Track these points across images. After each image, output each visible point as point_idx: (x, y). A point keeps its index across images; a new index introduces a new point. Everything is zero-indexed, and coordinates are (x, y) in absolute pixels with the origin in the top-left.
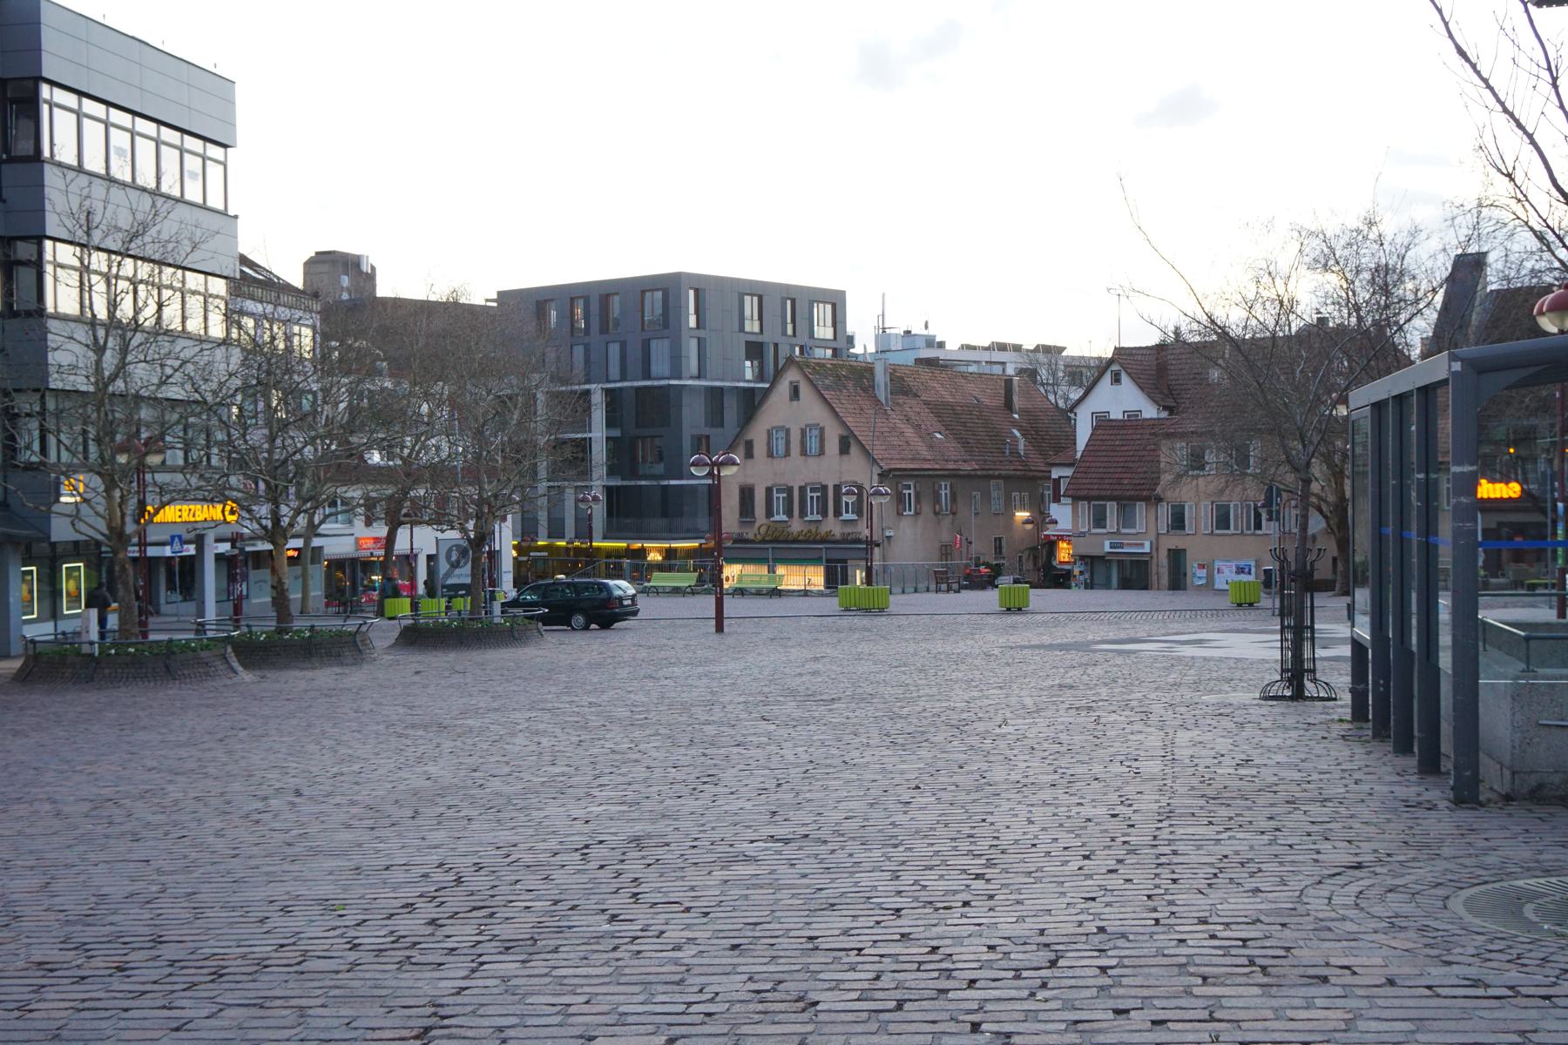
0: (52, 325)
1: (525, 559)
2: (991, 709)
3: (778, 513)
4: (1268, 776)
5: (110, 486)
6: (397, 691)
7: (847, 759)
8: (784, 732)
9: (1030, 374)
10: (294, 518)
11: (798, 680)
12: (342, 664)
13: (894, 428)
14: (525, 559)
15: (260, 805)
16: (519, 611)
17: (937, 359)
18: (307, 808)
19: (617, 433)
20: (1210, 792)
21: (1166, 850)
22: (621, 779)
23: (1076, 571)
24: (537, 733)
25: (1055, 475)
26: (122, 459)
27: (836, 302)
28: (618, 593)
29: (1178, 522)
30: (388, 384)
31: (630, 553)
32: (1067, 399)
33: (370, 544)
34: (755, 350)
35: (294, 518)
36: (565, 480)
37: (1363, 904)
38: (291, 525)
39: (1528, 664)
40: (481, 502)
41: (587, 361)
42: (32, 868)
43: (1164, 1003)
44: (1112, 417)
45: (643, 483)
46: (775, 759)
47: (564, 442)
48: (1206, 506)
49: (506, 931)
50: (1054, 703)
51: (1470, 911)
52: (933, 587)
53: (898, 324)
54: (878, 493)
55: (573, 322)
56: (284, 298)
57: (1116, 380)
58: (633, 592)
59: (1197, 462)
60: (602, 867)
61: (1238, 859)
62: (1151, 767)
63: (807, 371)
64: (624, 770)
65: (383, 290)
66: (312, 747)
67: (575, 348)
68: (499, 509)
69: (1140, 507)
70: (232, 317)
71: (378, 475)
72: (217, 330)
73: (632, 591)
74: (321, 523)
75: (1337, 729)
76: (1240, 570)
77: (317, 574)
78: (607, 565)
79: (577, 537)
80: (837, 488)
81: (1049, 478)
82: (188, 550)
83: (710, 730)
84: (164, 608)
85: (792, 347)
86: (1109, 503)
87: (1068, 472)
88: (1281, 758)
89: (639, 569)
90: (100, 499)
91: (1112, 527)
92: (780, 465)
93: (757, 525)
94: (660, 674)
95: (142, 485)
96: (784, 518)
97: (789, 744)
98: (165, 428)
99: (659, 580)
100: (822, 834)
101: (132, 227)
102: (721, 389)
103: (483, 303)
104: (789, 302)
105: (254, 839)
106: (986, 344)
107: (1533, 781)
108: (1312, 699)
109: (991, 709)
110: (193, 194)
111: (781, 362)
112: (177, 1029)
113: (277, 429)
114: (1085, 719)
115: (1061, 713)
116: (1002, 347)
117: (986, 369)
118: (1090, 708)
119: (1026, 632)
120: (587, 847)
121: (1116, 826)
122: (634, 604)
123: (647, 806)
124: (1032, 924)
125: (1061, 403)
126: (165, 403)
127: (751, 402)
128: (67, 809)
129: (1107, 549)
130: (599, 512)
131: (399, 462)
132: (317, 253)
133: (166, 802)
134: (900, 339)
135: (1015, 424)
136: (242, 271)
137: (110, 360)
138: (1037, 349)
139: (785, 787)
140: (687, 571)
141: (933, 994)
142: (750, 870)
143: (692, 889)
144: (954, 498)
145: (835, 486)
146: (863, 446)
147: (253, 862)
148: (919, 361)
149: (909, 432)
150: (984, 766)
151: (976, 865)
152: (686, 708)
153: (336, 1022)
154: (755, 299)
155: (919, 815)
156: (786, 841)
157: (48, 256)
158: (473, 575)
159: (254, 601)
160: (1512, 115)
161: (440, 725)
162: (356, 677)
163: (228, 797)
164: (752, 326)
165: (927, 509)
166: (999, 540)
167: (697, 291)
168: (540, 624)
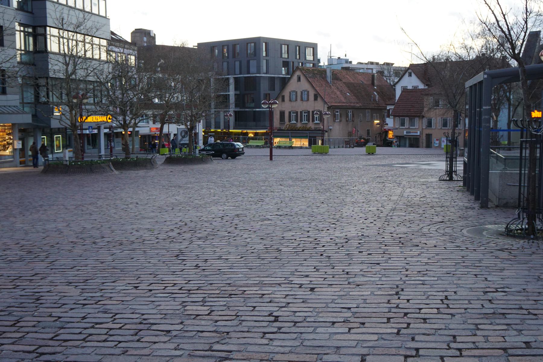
0: (51, 56)
1: (207, 135)
2: (352, 183)
3: (293, 121)
4: (429, 200)
5: (71, 109)
6: (166, 177)
7: (304, 196)
8: (286, 189)
9: (381, 73)
10: (130, 121)
11: (294, 175)
12: (147, 169)
13: (333, 92)
14: (207, 135)
15: (126, 207)
16: (205, 152)
17: (349, 67)
18: (141, 208)
19: (238, 92)
20: (409, 204)
21: (389, 218)
22: (234, 200)
23: (394, 141)
24: (210, 188)
25: (388, 108)
26: (75, 101)
27: (314, 47)
28: (237, 147)
29: (430, 124)
30: (161, 76)
31: (242, 134)
32: (394, 82)
33: (155, 130)
34: (286, 64)
35: (130, 121)
36: (220, 109)
37: (438, 230)
38: (130, 123)
39: (505, 166)
40: (192, 116)
41: (228, 68)
42: (62, 221)
43: (373, 250)
44: (408, 88)
45: (247, 110)
46: (282, 195)
47: (220, 96)
48: (439, 119)
49: (199, 235)
50: (373, 181)
51: (468, 233)
52: (344, 146)
54: (326, 114)
55: (223, 54)
56: (126, 46)
57: (410, 75)
58: (243, 146)
59: (437, 104)
60: (227, 221)
61: (409, 220)
62: (394, 198)
63: (303, 71)
64: (235, 198)
65: (158, 42)
66: (140, 192)
67: (224, 63)
68: (198, 118)
69: (417, 120)
70: (108, 52)
71: (157, 106)
72: (104, 57)
73: (242, 146)
74: (139, 122)
75: (457, 188)
77: (137, 140)
78: (235, 138)
79: (225, 128)
81: (386, 109)
82: (94, 131)
83: (263, 188)
84: (87, 151)
85: (299, 63)
86: (406, 118)
87: (392, 107)
88: (435, 196)
89: (245, 138)
90: (68, 114)
91: (407, 126)
92: (294, 104)
93: (286, 125)
94: (250, 173)
95: (81, 109)
96: (295, 122)
97: (287, 192)
98: (87, 91)
99: (251, 143)
100: (291, 214)
101: (77, 24)
102: (274, 77)
103: (192, 47)
104: (298, 47)
105: (126, 214)
106: (366, 62)
107: (505, 201)
108: (455, 180)
109: (352, 183)
110: (95, 11)
111: (295, 68)
112: (112, 255)
113: (124, 91)
114: (381, 186)
115: (374, 184)
116: (372, 63)
117: (366, 71)
118: (383, 182)
119: (373, 161)
120: (223, 217)
121: (377, 212)
122: (243, 150)
123: (241, 207)
124: (344, 234)
125: (392, 83)
126: (88, 82)
127: (284, 82)
128: (68, 207)
129: (405, 134)
130: (232, 120)
131: (164, 102)
132: (136, 29)
133: (98, 206)
134: (336, 60)
135: (375, 90)
136: (112, 37)
137: (70, 68)
138: (384, 64)
139: (283, 202)
140: (262, 140)
141: (313, 248)
142: (269, 222)
143: (252, 226)
144: (353, 116)
146: (322, 98)
147: (127, 220)
148: (343, 68)
149: (338, 93)
150: (344, 197)
151: (333, 221)
152: (257, 182)
153: (154, 254)
154: (286, 46)
155: (321, 210)
156: (281, 216)
157: (48, 32)
158: (189, 140)
159: (116, 149)
160: (488, 5)
161: (179, 186)
162: (152, 173)
163: (116, 205)
164: (285, 56)
165: (344, 119)
166: (368, 131)
167: (266, 43)
168: (212, 157)
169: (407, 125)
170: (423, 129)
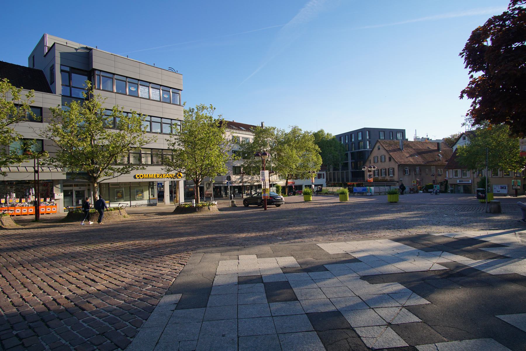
27: (403, 132)
53: (420, 136)
76: (502, 188)
80: (389, 169)
104: (391, 133)
129: (458, 182)
135: (440, 153)
144: (420, 171)
145: (388, 169)
167: (369, 131)
169: (459, 175)
170: (474, 178)
